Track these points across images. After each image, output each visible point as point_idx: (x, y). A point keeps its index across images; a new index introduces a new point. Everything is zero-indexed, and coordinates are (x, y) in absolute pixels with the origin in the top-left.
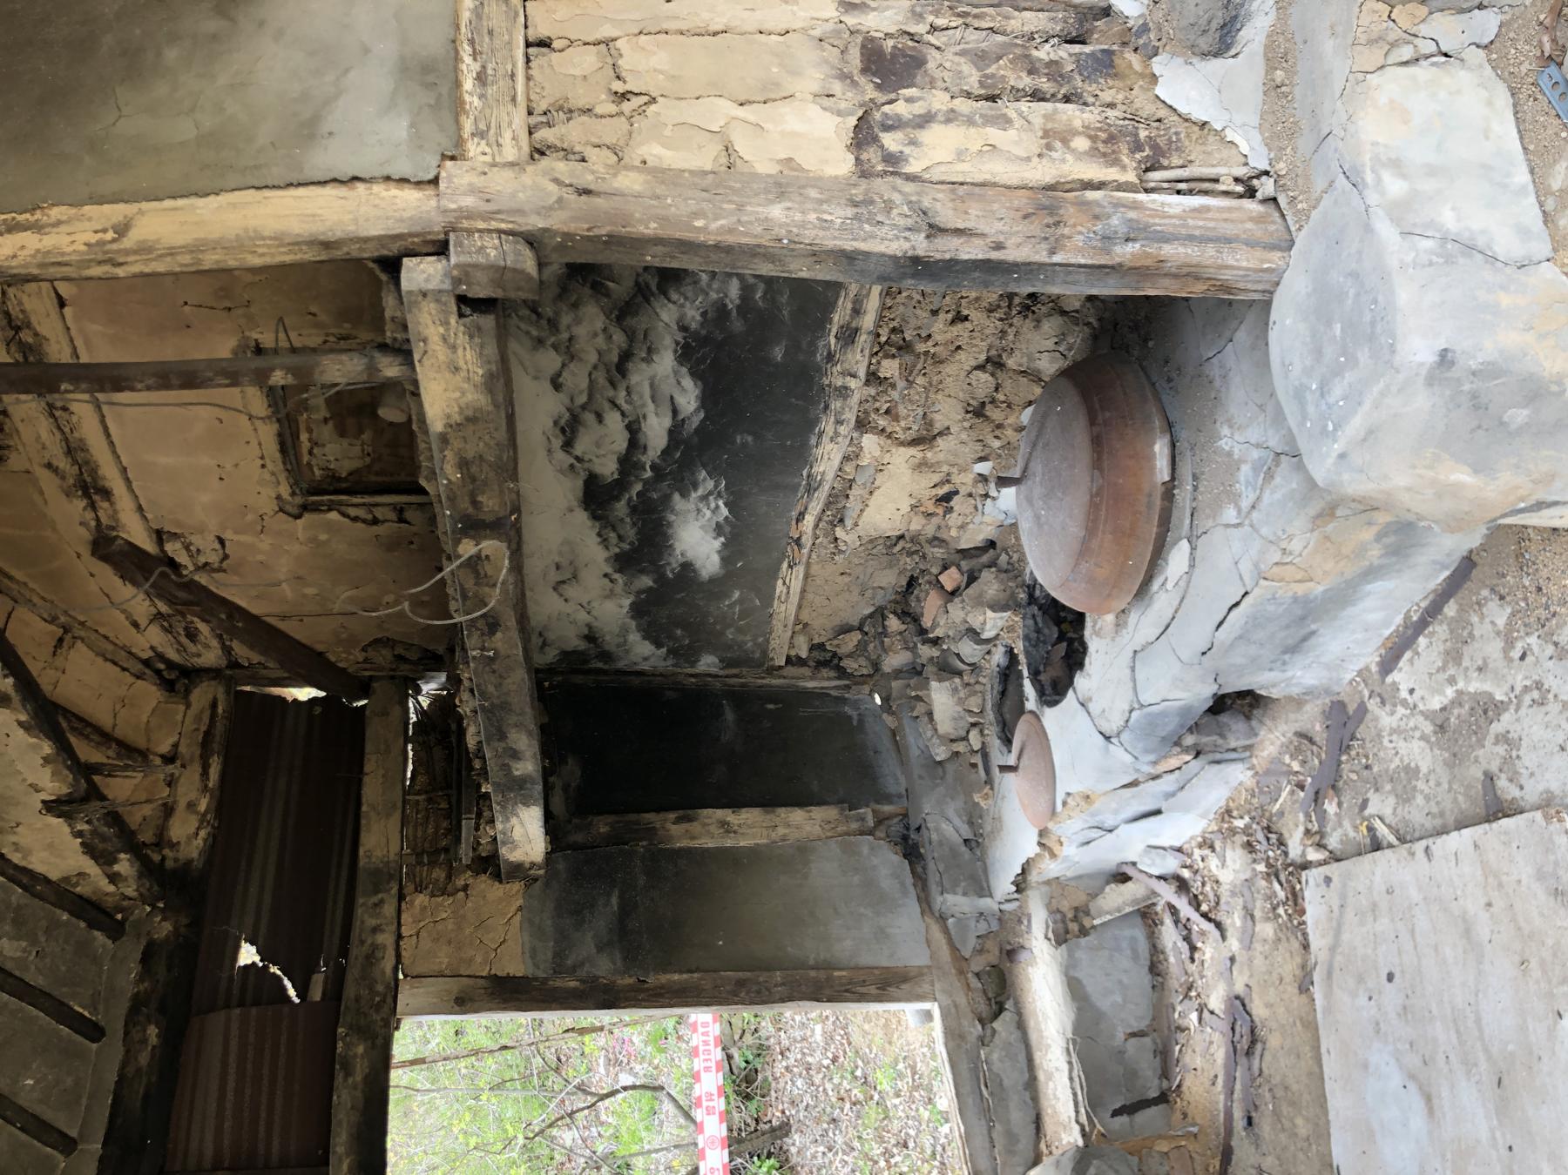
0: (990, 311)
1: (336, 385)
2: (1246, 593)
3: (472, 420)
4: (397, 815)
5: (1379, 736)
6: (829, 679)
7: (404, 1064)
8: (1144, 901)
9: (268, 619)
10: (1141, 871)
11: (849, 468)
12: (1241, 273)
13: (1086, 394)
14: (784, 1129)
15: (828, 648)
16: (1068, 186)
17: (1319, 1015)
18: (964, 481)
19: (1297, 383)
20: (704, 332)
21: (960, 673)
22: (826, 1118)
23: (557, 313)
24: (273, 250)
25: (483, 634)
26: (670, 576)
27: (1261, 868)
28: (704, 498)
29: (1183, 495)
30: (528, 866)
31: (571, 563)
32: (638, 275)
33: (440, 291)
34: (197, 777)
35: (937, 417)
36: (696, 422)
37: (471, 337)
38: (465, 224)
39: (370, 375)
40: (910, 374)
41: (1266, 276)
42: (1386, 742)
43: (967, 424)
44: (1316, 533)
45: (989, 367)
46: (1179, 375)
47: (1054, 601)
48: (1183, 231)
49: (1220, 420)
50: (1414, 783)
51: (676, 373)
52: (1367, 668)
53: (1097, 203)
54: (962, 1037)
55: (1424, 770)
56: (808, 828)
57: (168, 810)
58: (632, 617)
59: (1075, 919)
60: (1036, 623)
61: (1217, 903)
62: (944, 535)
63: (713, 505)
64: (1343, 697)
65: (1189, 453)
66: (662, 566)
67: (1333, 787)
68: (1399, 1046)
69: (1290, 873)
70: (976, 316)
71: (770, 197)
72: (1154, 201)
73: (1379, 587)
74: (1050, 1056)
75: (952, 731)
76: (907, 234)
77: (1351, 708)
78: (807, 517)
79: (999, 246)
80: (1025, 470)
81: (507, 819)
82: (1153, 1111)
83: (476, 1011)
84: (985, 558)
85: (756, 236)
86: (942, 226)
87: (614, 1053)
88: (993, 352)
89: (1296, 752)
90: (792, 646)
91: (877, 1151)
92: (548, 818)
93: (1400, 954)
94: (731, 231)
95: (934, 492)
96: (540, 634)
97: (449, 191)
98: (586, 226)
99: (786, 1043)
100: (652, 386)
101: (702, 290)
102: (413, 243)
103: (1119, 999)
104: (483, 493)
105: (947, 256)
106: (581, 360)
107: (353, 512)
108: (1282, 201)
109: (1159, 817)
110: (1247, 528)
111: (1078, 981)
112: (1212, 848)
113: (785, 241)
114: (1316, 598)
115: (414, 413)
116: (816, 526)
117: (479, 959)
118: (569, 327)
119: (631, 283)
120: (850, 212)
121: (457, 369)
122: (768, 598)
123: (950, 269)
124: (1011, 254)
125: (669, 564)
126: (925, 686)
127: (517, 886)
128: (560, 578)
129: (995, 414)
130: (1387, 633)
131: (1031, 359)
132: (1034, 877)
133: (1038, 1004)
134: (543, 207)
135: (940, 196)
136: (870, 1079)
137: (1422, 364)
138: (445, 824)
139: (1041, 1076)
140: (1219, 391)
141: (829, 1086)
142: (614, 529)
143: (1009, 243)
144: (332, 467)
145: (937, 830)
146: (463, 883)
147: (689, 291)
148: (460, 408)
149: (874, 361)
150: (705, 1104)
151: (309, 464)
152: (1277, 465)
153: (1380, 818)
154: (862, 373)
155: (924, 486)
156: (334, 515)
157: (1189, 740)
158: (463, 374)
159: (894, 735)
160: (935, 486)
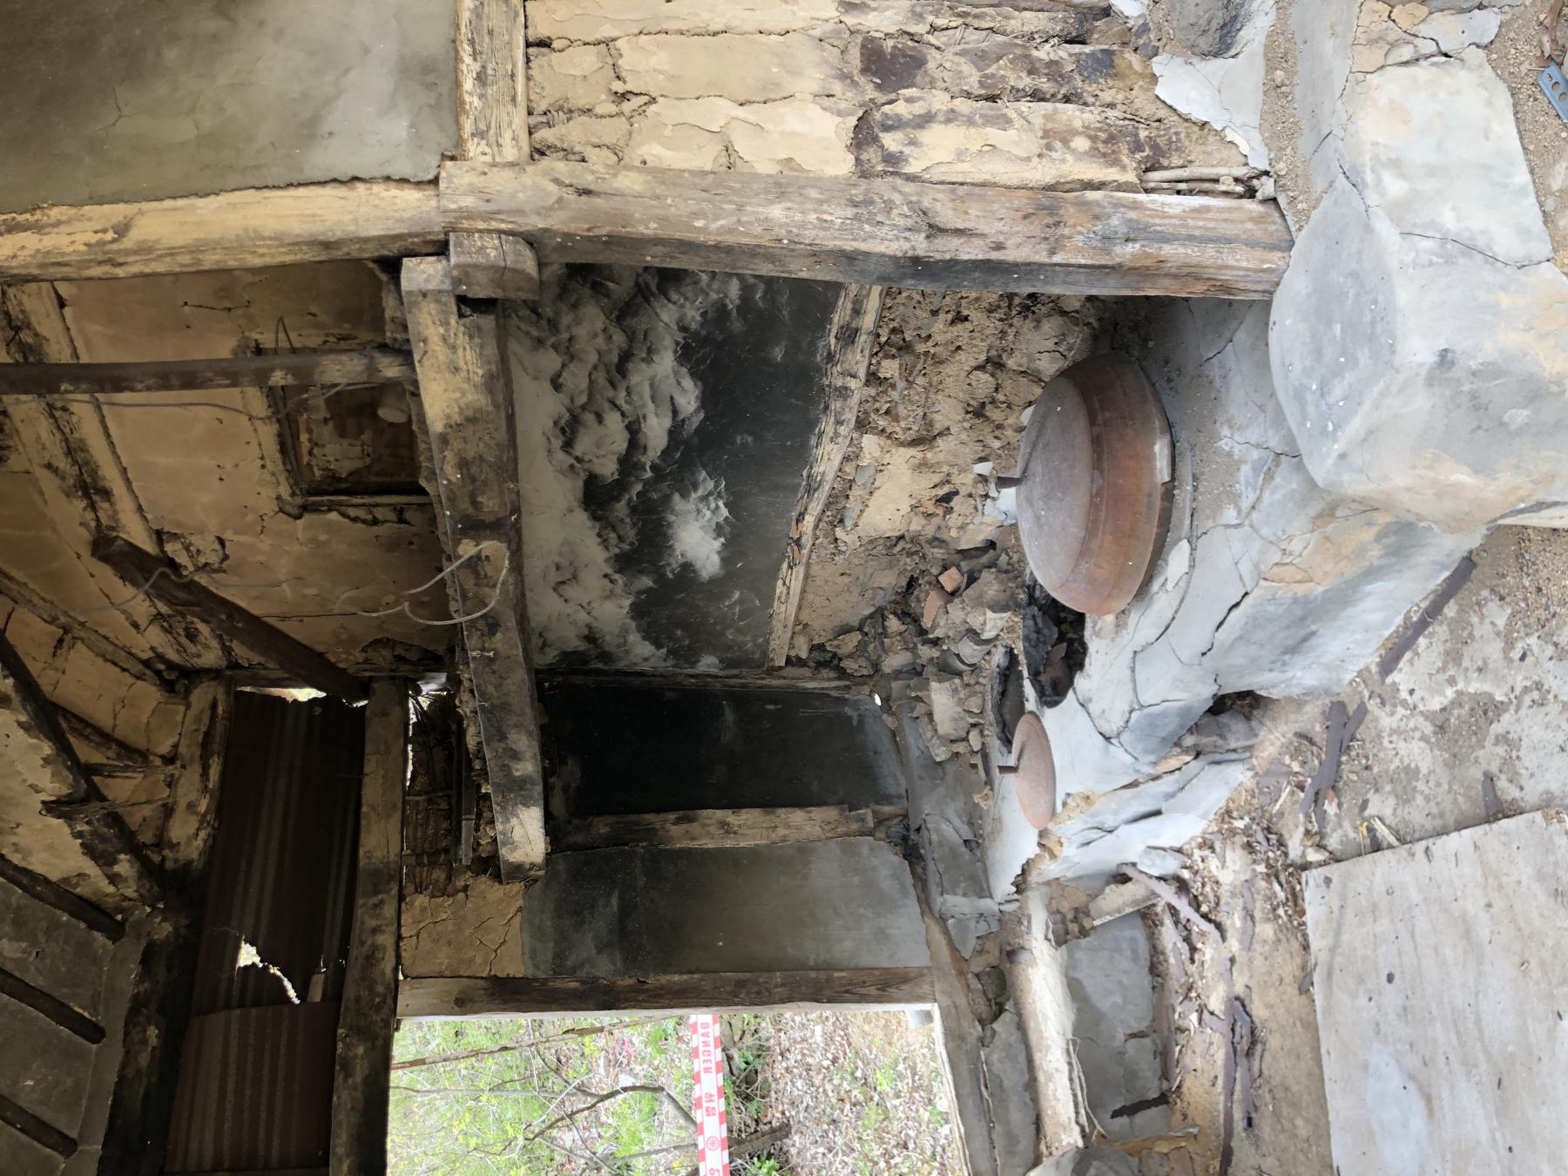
0: (990, 311)
1: (336, 385)
2: (1246, 594)
3: (472, 420)
4: (397, 816)
5: (1379, 736)
6: (829, 679)
7: (404, 1065)
8: (1144, 901)
9: (268, 620)
10: (1141, 872)
11: (849, 468)
12: (1241, 273)
13: (1086, 395)
14: (784, 1130)
15: (828, 648)
16: (1068, 187)
17: (1319, 1016)
18: (964, 481)
19: (1297, 383)
20: (704, 332)
21: (960, 674)
22: (826, 1119)
23: (557, 314)
24: (273, 251)
25: (483, 635)
26: (670, 576)
27: (1261, 868)
28: (704, 498)
29: (1183, 495)
30: (528, 867)
31: (571, 564)
32: (638, 275)
33: (440, 292)
34: (197, 777)
35: (937, 417)
36: (696, 422)
37: (471, 337)
38: (465, 224)
39: (370, 375)
40: (910, 375)
41: (1266, 277)
42: (1386, 742)
43: (967, 425)
44: (1316, 534)
45: (989, 367)
46: (1179, 375)
47: (1054, 602)
48: (1183, 232)
49: (1220, 420)
50: (1414, 783)
51: (676, 373)
52: (1367, 669)
53: (1097, 203)
54: (962, 1038)
55: (1424, 770)
56: (808, 829)
57: (168, 811)
58: (632, 618)
59: (1075, 920)
60: (1036, 624)
61: (1217, 904)
62: (944, 536)
63: (713, 506)
64: (1343, 698)
65: (1189, 454)
66: (662, 566)
67: (1333, 788)
68: (1399, 1047)
69: (1290, 874)
70: (976, 316)
71: (770, 197)
72: (1154, 201)
73: (1379, 587)
74: (1050, 1057)
75: (952, 731)
76: (907, 234)
77: (1351, 709)
78: (807, 517)
79: (999, 247)
80: (1025, 471)
81: (507, 820)
82: (1153, 1112)
83: (476, 1012)
84: (985, 559)
85: (756, 236)
86: (942, 226)
87: (614, 1054)
88: (993, 353)
89: (1296, 753)
90: (792, 646)
91: (877, 1152)
92: (548, 818)
93: (1400, 954)
94: (731, 231)
95: (934, 492)
96: (540, 635)
97: (449, 191)
98: (586, 226)
99: (786, 1044)
100: (652, 386)
101: (702, 291)
102: (413, 243)
103: (1119, 1000)
104: (483, 493)
105: (947, 257)
106: (581, 360)
107: (353, 512)
108: (1282, 201)
109: (1159, 818)
110: (1247, 529)
111: (1078, 982)
112: (1212, 848)
113: (785, 242)
114: (1316, 598)
115: (414, 413)
116: (816, 527)
117: (479, 960)
118: (569, 327)
119: (631, 284)
120: (850, 212)
121: (457, 369)
122: (768, 599)
123: (950, 269)
124: (1011, 255)
125: (669, 564)
126: (925, 686)
127: (517, 887)
128: (560, 579)
129: (995, 414)
130: (1387, 633)
131: (1031, 359)
132: (1034, 878)
133: (1038, 1005)
134: (543, 207)
135: (940, 196)
136: (870, 1080)
137: (1422, 365)
138: (445, 825)
139: (1041, 1077)
140: (1219, 391)
141: (829, 1087)
142: (614, 529)
143: (1009, 244)
144: (332, 467)
145: (937, 830)
146: (463, 884)
147: (689, 291)
148: (460, 408)
149: (874, 361)
150: (705, 1105)
151: (309, 464)
152: (1277, 466)
153: (1380, 819)
154: (862, 374)
155: (924, 487)
156: (334, 516)
157: (1189, 741)
158: (463, 374)
159: (894, 735)
160: (935, 487)
